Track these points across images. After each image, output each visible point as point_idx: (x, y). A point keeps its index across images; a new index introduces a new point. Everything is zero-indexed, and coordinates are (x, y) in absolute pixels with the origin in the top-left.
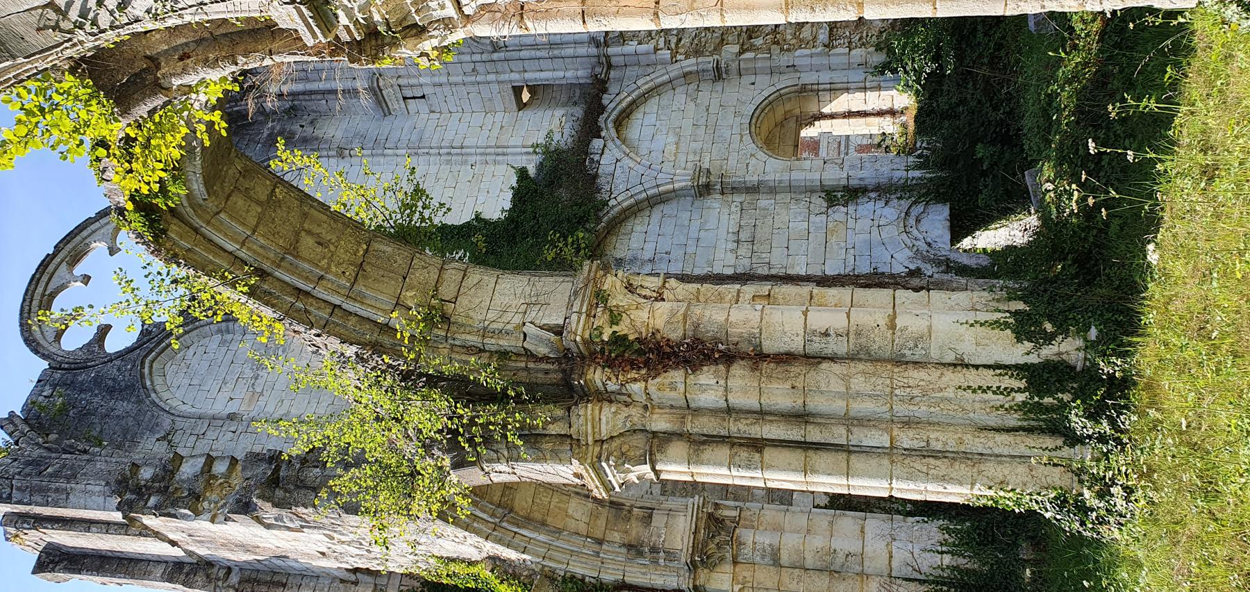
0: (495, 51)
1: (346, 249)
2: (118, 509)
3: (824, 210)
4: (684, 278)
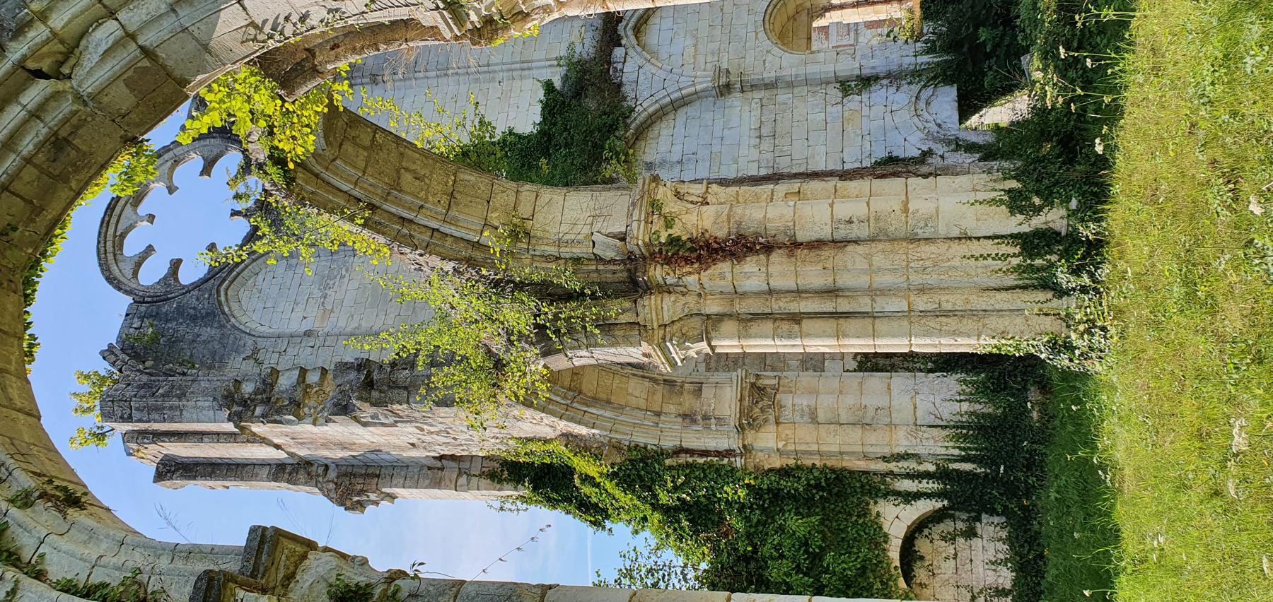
2: (229, 420)
4: (723, 183)
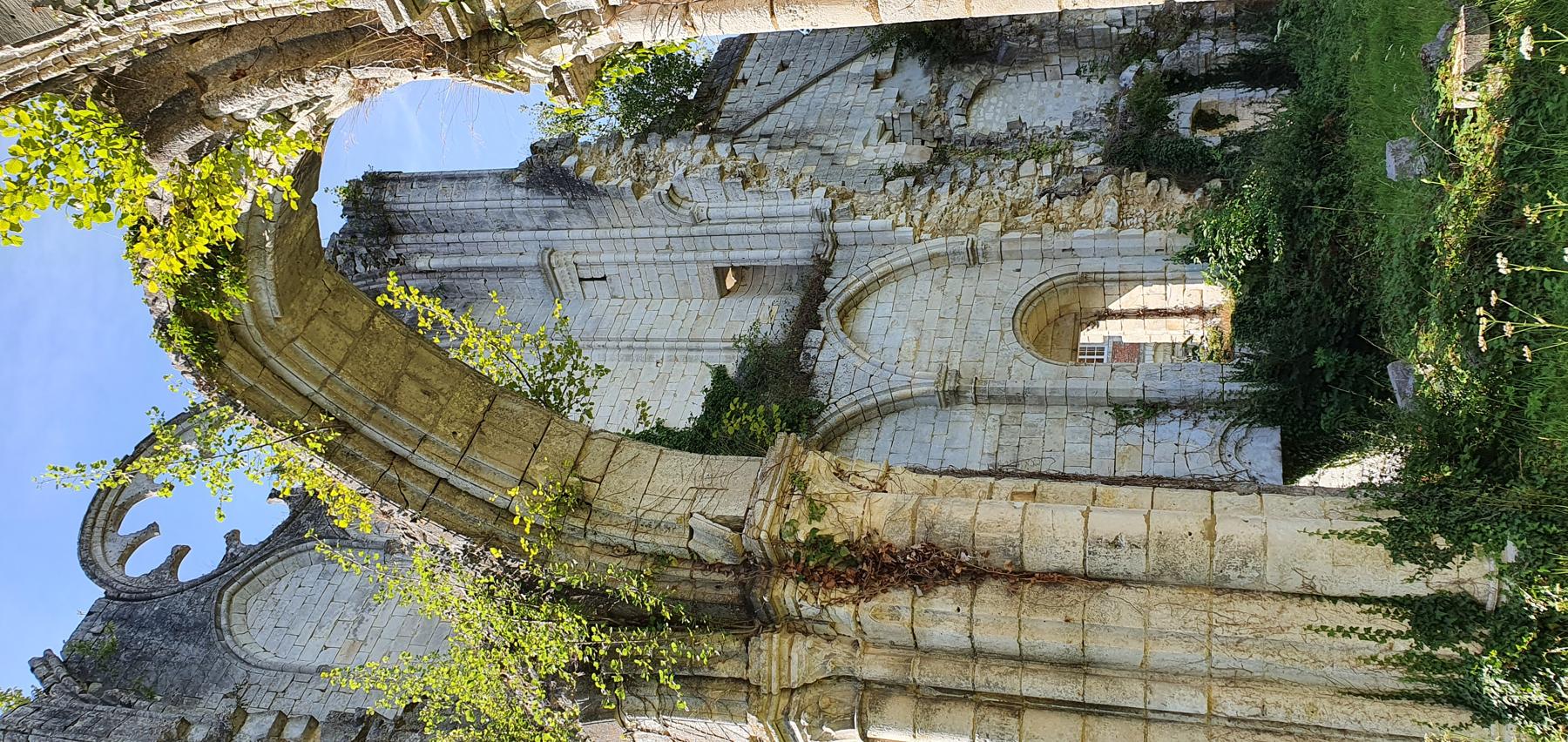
0: (695, 224)
1: (461, 405)
3: (1111, 429)
